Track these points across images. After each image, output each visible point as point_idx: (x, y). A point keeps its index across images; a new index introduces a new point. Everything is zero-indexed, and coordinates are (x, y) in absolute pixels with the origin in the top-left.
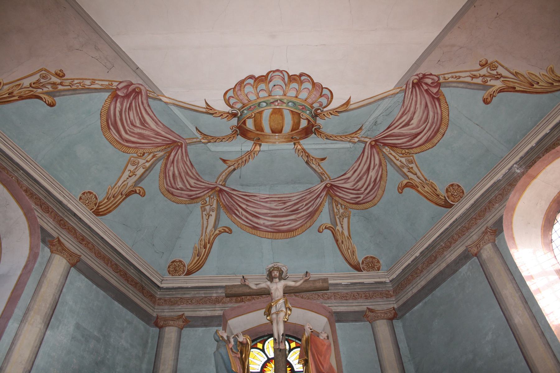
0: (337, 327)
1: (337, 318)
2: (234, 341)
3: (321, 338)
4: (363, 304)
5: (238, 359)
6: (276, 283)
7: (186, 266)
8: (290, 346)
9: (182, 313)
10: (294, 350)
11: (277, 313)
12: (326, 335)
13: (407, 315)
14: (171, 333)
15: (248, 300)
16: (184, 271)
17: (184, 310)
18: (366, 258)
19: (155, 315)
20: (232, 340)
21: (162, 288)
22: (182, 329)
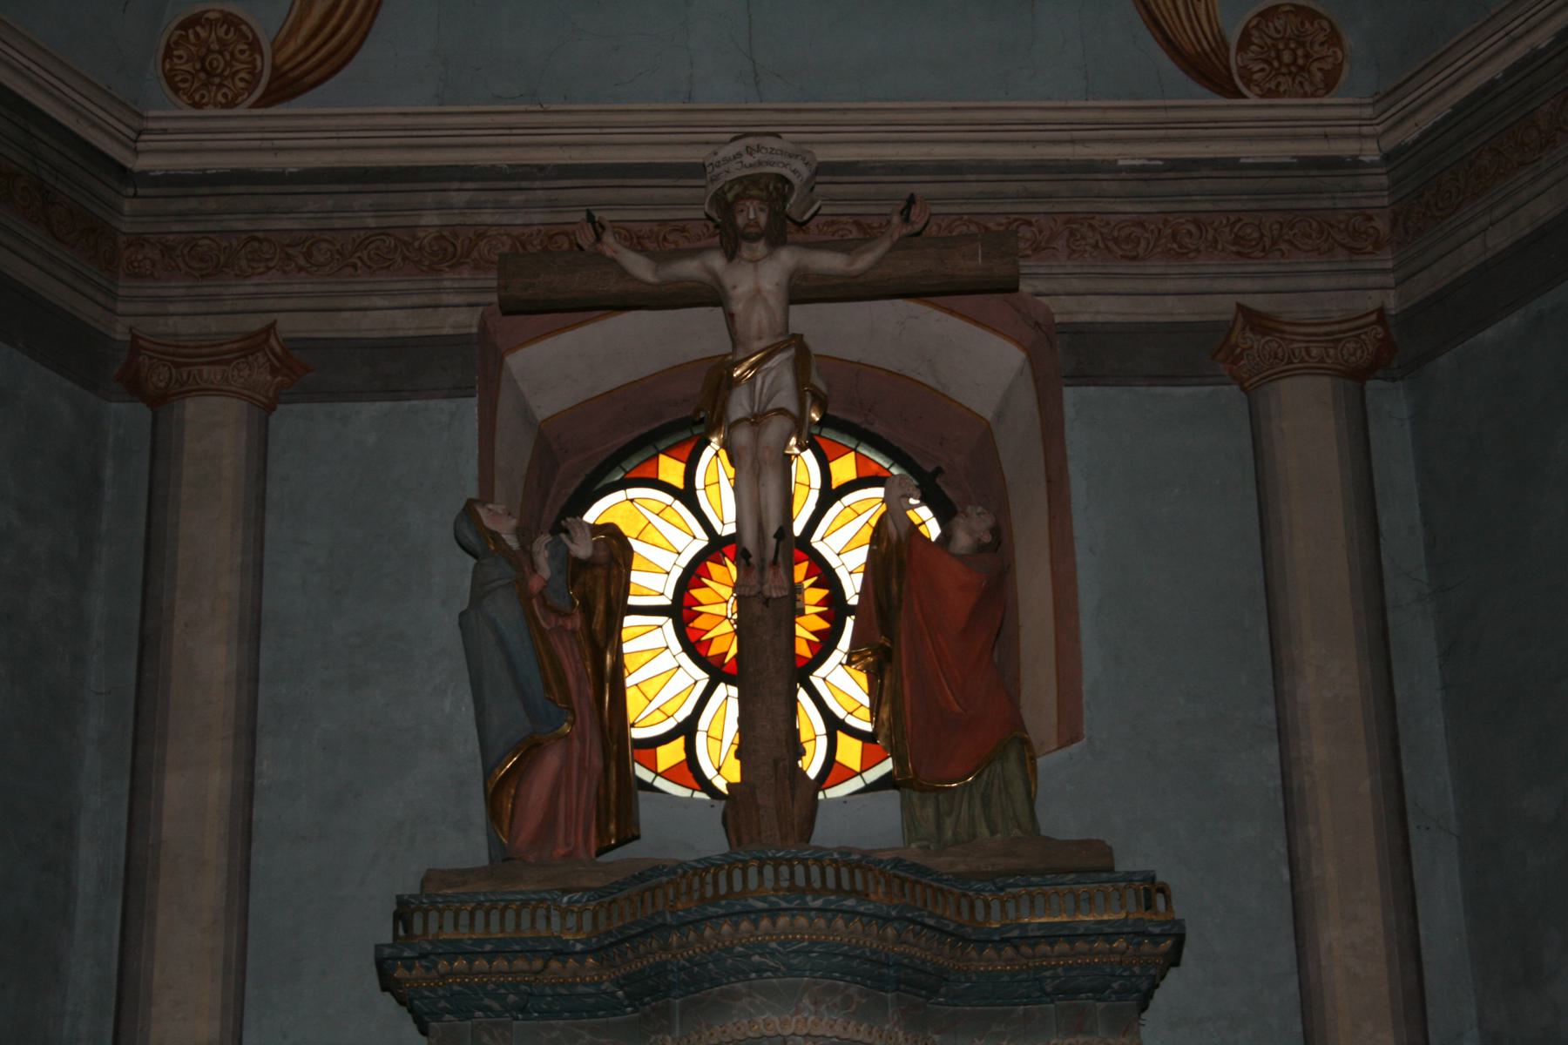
0: (1069, 411)
1: (1072, 357)
6: (755, 262)
8: (826, 475)
9: (266, 319)
10: (849, 499)
14: (213, 427)
16: (255, 76)
17: (269, 304)
18: (1267, 15)
19: (120, 332)
21: (144, 178)
22: (270, 409)
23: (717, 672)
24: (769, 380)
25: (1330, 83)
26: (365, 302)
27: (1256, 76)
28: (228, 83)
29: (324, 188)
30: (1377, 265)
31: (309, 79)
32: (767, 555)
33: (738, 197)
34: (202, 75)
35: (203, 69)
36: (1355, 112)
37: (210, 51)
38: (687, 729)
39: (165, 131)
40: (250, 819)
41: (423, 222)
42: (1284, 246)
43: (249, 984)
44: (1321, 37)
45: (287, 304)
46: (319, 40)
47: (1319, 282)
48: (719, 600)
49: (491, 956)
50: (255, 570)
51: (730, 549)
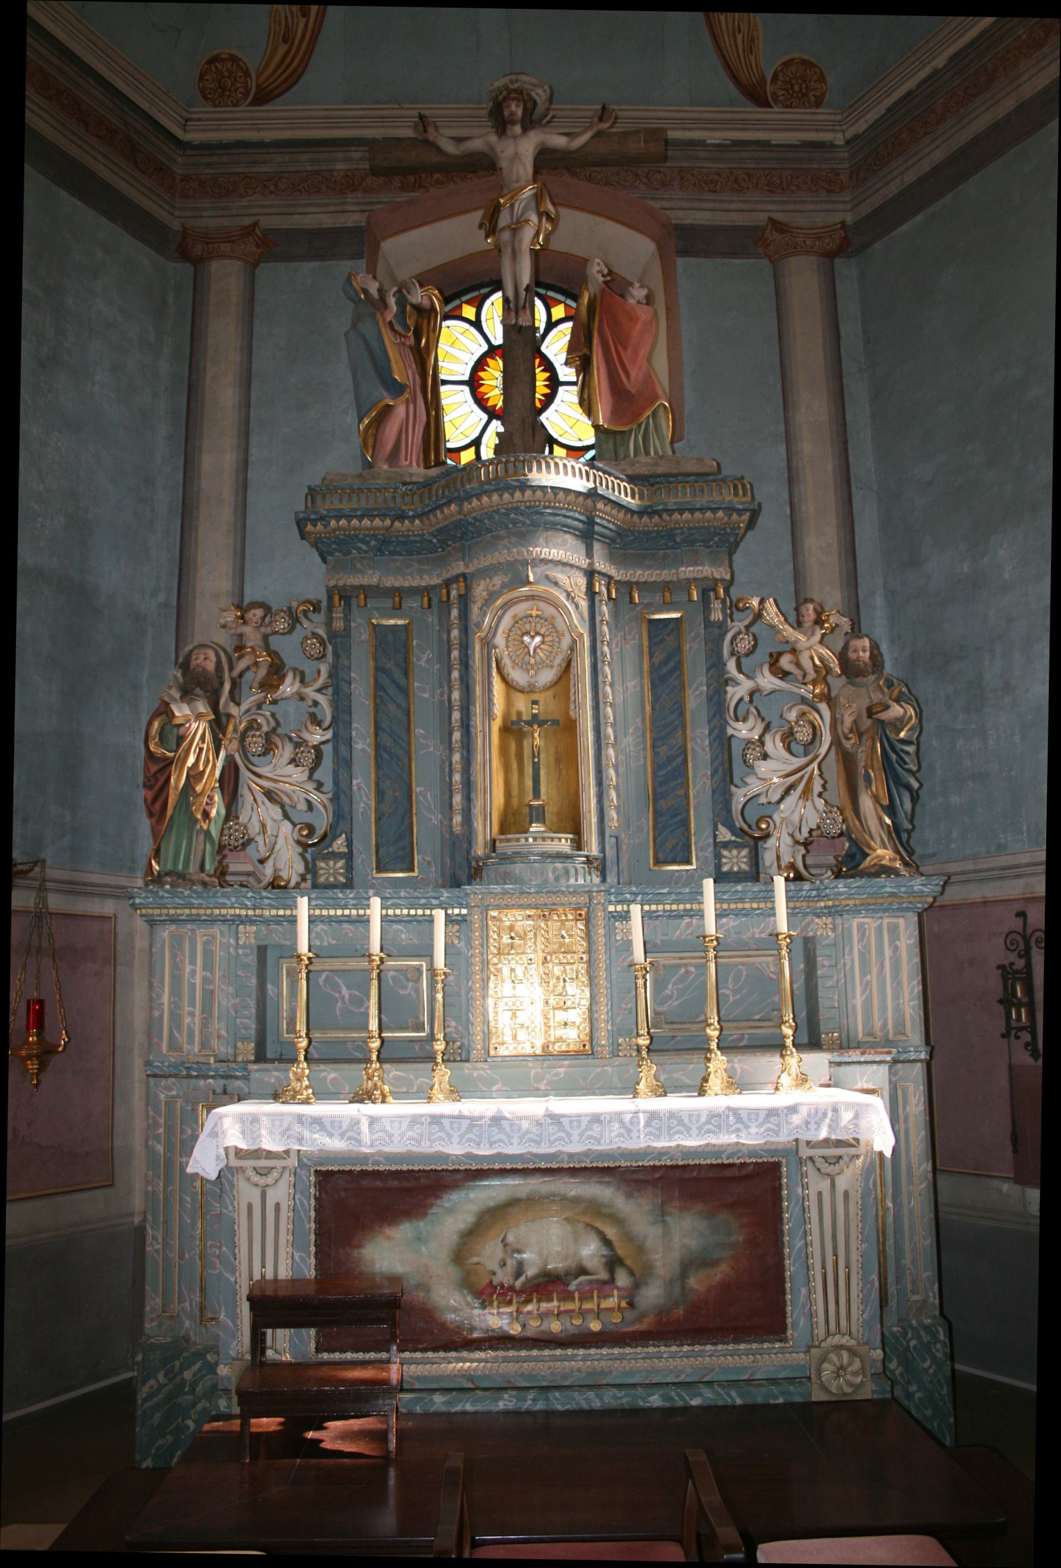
0: (679, 270)
2: (397, 303)
3: (631, 301)
4: (759, 207)
5: (408, 352)
6: (515, 137)
7: (254, 77)
8: (549, 315)
9: (253, 219)
11: (516, 228)
12: (644, 292)
13: (878, 245)
14: (226, 276)
15: (437, 182)
16: (248, 91)
17: (255, 211)
18: (787, 64)
19: (176, 225)
20: (392, 301)
22: (255, 265)
23: (493, 415)
24: (522, 205)
25: (818, 104)
26: (306, 210)
27: (781, 98)
28: (233, 94)
29: (283, 150)
30: (841, 199)
31: (277, 92)
32: (520, 349)
33: (505, 98)
34: (220, 90)
35: (220, 87)
36: (832, 117)
37: (223, 76)
38: (476, 443)
39: (199, 120)
40: (246, 479)
41: (337, 167)
42: (794, 188)
43: (247, 562)
44: (815, 78)
45: (266, 211)
46: (280, 71)
47: (811, 207)
48: (493, 377)
49: (360, 518)
50: (248, 350)
51: (500, 351)
